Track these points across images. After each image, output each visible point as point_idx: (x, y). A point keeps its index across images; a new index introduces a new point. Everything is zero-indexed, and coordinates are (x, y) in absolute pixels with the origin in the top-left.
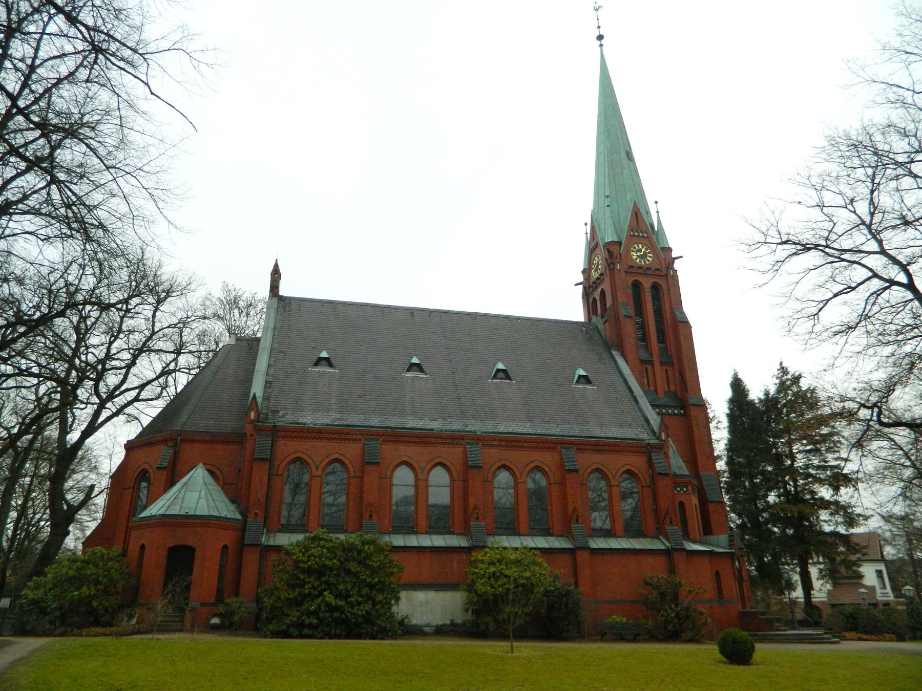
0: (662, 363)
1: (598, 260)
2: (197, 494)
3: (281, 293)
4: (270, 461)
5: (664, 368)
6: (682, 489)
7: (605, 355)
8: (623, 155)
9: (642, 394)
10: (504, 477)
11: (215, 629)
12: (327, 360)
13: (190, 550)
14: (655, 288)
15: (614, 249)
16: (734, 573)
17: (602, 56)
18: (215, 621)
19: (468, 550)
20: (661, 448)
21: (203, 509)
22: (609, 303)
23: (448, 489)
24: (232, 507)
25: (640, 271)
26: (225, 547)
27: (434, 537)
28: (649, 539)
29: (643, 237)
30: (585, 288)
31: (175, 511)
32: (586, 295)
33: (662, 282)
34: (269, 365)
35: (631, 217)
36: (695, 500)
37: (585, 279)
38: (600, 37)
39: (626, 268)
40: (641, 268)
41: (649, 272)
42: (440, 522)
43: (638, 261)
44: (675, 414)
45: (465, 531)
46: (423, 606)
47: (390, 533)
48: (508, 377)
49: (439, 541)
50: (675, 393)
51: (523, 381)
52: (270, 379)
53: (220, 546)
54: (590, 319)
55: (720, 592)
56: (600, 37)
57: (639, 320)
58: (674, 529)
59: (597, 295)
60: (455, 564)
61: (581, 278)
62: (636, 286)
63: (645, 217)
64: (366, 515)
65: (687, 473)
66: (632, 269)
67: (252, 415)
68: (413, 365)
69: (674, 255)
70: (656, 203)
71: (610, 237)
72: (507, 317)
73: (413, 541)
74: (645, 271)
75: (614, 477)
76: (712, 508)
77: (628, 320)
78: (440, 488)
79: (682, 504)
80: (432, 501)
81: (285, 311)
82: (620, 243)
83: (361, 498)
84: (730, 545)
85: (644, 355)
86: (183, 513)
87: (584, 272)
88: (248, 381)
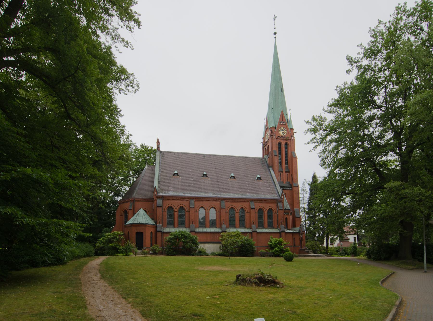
0: (286, 172)
1: (268, 133)
4: (162, 207)
7: (267, 170)
8: (280, 90)
11: (151, 254)
12: (177, 174)
13: (142, 233)
14: (286, 144)
15: (273, 130)
18: (151, 252)
19: (220, 232)
20: (281, 201)
21: (144, 222)
22: (270, 150)
23: (215, 215)
24: (152, 221)
25: (282, 138)
26: (151, 232)
31: (136, 222)
32: (263, 147)
33: (289, 142)
34: (159, 176)
36: (291, 217)
38: (275, 34)
41: (285, 138)
42: (213, 224)
45: (221, 227)
46: (209, 248)
47: (198, 228)
48: (178, 175)
49: (212, 230)
50: (289, 182)
52: (159, 181)
54: (264, 156)
55: (294, 244)
58: (282, 226)
59: (266, 147)
61: (262, 141)
62: (280, 144)
63: (285, 116)
64: (191, 223)
65: (289, 208)
69: (294, 131)
71: (272, 125)
72: (236, 157)
73: (205, 230)
74: (283, 138)
76: (296, 219)
77: (276, 157)
78: (213, 215)
79: (286, 218)
80: (210, 219)
82: (275, 127)
83: (189, 218)
85: (281, 170)
86: (138, 223)
87: (263, 138)
88: (153, 181)
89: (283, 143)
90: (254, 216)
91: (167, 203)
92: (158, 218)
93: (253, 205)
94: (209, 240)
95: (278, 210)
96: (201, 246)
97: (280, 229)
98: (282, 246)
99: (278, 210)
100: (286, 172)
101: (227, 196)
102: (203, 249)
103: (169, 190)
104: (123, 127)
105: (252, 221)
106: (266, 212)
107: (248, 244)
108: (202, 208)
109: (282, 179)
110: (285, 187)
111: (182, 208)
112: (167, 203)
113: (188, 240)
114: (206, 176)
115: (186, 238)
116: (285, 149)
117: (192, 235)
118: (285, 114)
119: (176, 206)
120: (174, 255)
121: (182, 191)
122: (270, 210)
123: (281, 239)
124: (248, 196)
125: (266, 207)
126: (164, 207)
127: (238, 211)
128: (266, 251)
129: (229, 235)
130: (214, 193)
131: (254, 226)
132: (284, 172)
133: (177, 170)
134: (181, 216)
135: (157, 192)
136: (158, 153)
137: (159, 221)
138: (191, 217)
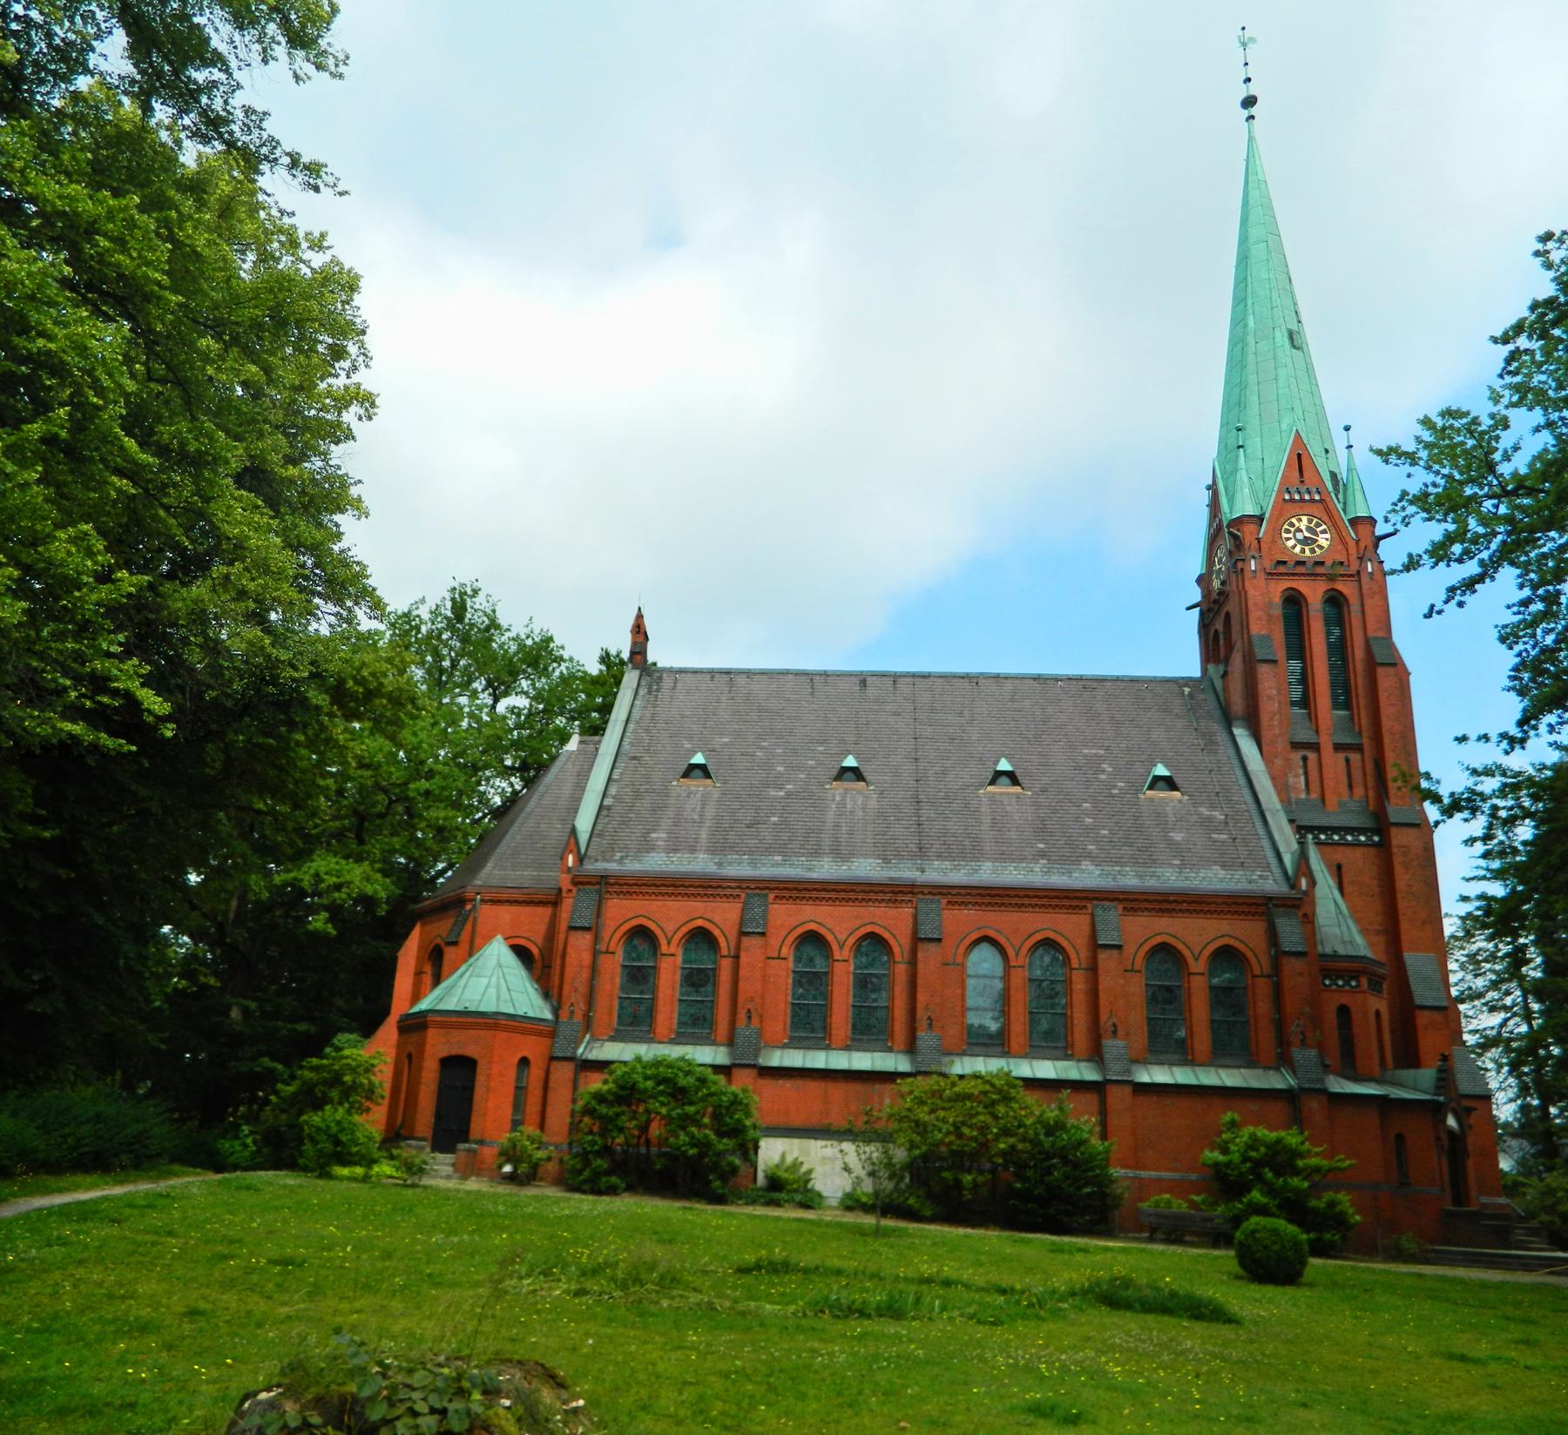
2: (485, 981)
3: (650, 659)
5: (1341, 756)
6: (1347, 983)
7: (1221, 736)
8: (1282, 339)
9: (1278, 806)
10: (984, 962)
12: (703, 768)
14: (1335, 601)
16: (1438, 1139)
17: (1251, 139)
25: (1300, 569)
26: (524, 1062)
27: (1035, 1063)
28: (1260, 1072)
29: (1312, 501)
30: (1202, 614)
31: (450, 1004)
32: (1204, 626)
35: (1288, 464)
36: (1379, 1004)
37: (1204, 596)
38: (1249, 102)
39: (1269, 565)
40: (1301, 563)
41: (1320, 570)
43: (1298, 550)
44: (1361, 844)
47: (963, 1054)
48: (708, 775)
49: (862, 1061)
51: (1044, 790)
53: (516, 1060)
56: (1249, 102)
57: (1296, 665)
59: (1219, 625)
60: (887, 1102)
61: (1196, 595)
62: (1294, 601)
66: (1283, 567)
67: (571, 860)
68: (1157, 779)
70: (1347, 429)
73: (818, 1059)
75: (841, 948)
76: (1423, 1018)
79: (1344, 1011)
81: (649, 692)
82: (1261, 519)
84: (1437, 1087)
85: (1304, 735)
86: (460, 1008)
88: (574, 809)
89: (1314, 593)
90: (1126, 992)
91: (621, 912)
92: (566, 988)
93: (1112, 924)
94: (837, 1120)
95: (1278, 955)
96: (772, 1152)
97: (1294, 1072)
98: (1295, 1182)
99: (1278, 955)
100: (1338, 747)
101: (958, 875)
102: (796, 1165)
103: (647, 847)
104: (1508, 637)
105: (1103, 1017)
106: (1198, 966)
107: (1062, 1154)
108: (985, 947)
109: (1315, 785)
110: (1335, 830)
111: (701, 937)
112: (621, 912)
113: (691, 1109)
114: (856, 774)
115: (679, 1094)
116: (1328, 622)
117: (742, 1084)
118: (1315, 450)
119: (670, 928)
120: (612, 1191)
121: (712, 851)
122: (1226, 955)
123: (1292, 1138)
124: (1088, 876)
125: (1197, 936)
126: (606, 934)
127: (846, 953)
128: (1193, 1205)
129: (937, 1094)
130: (886, 860)
131: (1304, 1056)
132: (1327, 749)
133: (709, 752)
134: (696, 979)
135: (581, 859)
136: (630, 678)
137: (575, 998)
138: (742, 985)
